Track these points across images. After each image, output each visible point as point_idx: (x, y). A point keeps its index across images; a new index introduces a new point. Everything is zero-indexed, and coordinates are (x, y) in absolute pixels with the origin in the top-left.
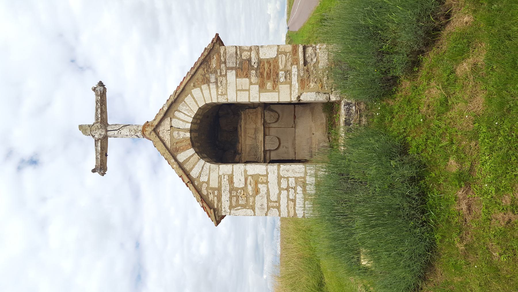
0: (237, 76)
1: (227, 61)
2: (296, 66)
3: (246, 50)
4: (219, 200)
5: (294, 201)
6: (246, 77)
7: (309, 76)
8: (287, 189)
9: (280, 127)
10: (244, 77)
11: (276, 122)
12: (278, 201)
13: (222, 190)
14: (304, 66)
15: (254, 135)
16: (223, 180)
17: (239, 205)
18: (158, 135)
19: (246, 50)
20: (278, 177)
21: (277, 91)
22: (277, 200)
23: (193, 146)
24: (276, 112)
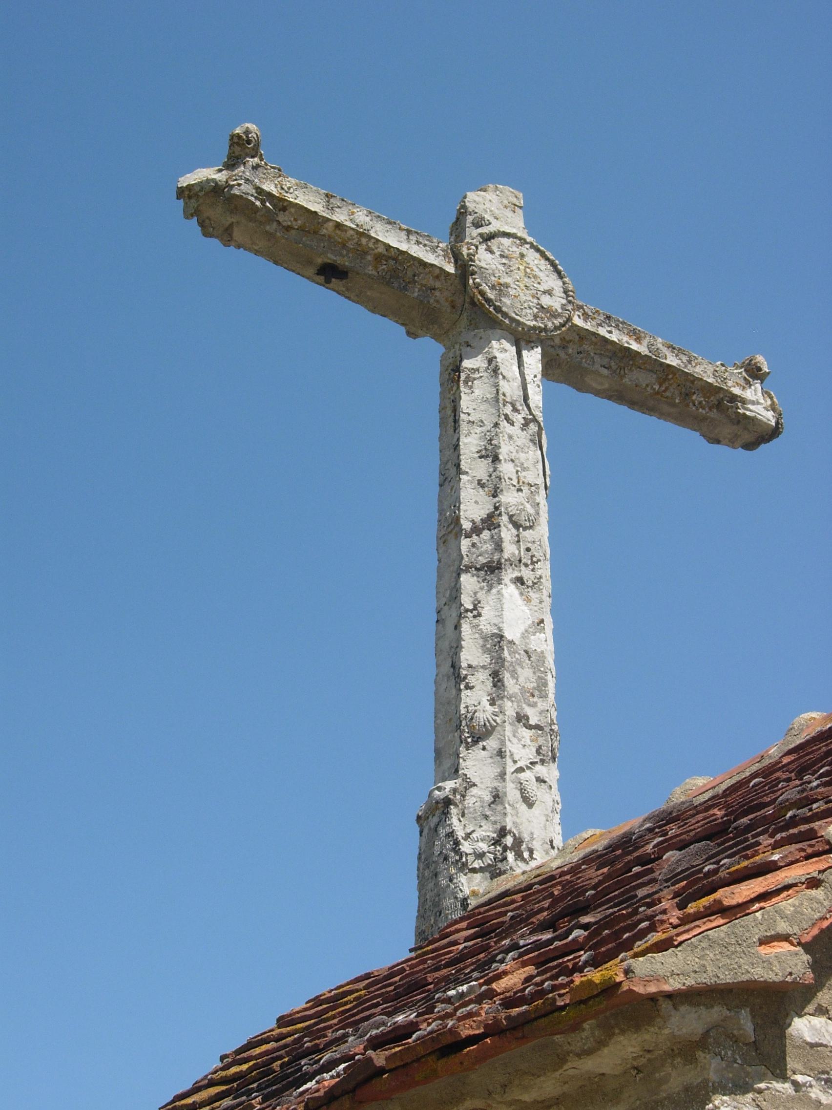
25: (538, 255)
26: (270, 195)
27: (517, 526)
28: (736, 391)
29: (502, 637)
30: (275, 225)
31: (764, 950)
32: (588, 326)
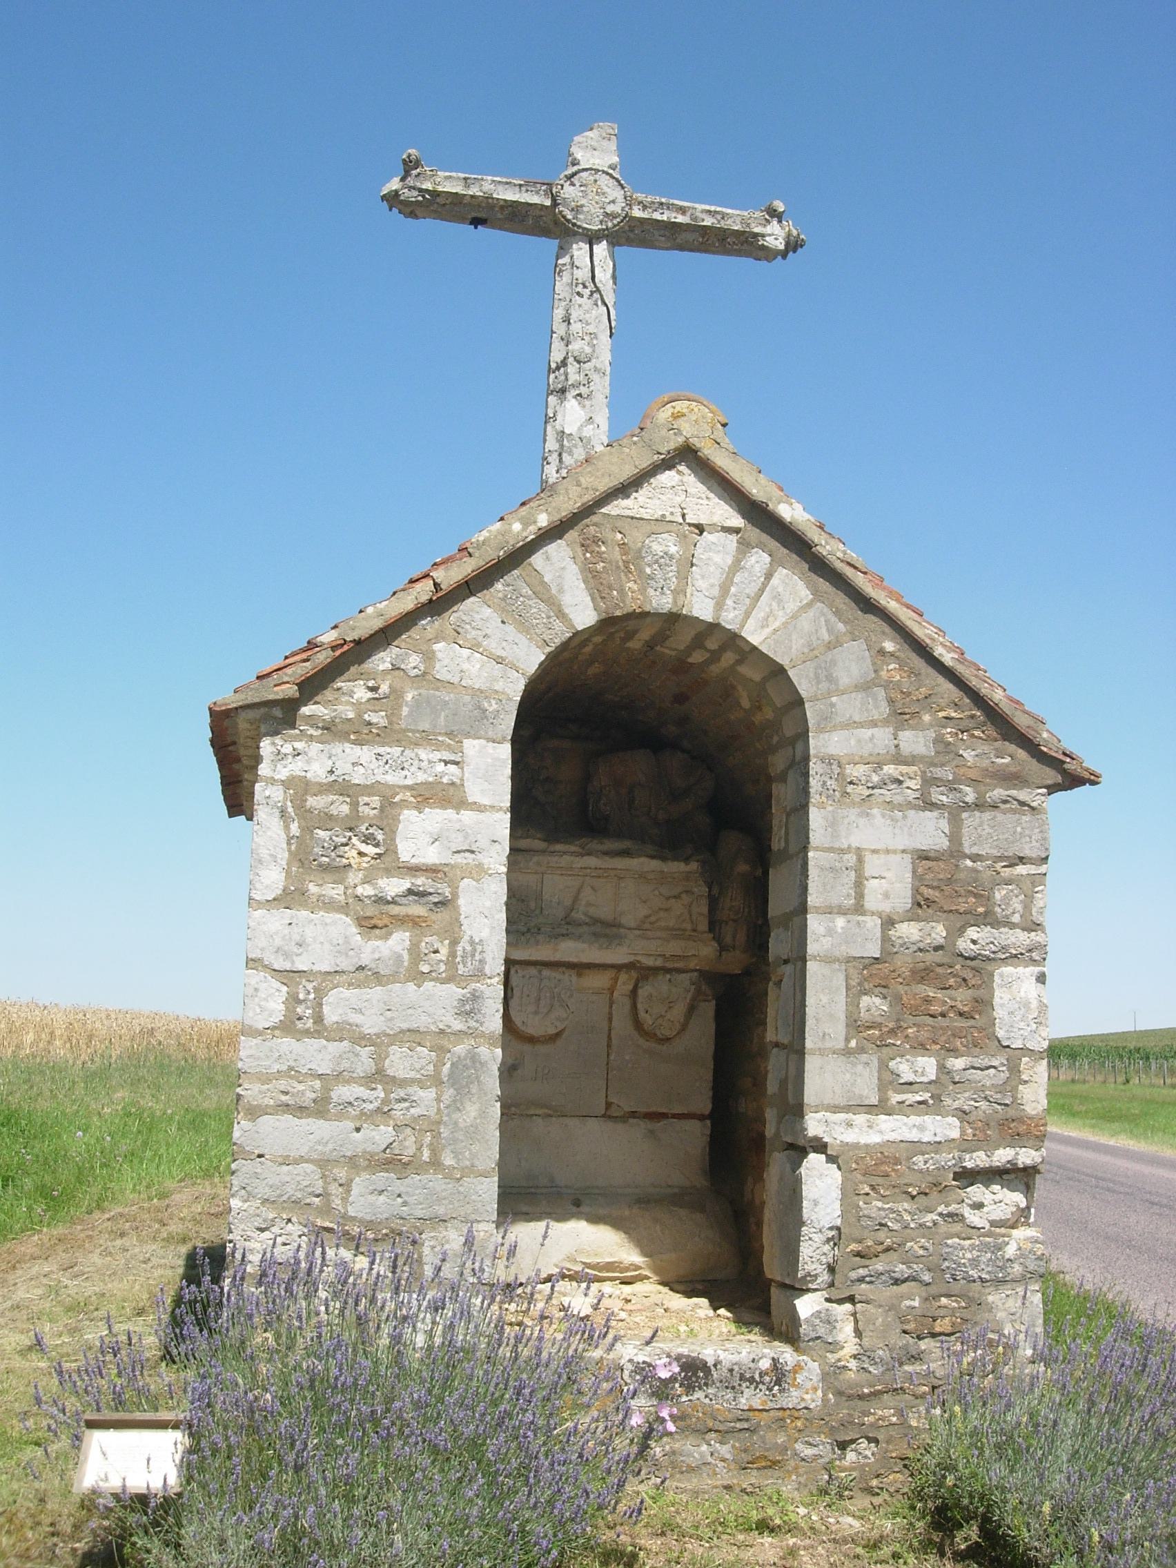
0: (923, 856)
1: (987, 815)
2: (955, 1134)
3: (1027, 906)
4: (331, 730)
5: (320, 1108)
6: (919, 897)
7: (913, 1197)
8: (378, 1076)
9: (609, 1046)
10: (916, 891)
11: (638, 1024)
12: (320, 1029)
13: (388, 749)
14: (955, 1173)
15: (585, 914)
16: (439, 757)
17: (308, 830)
18: (667, 464)
19: (1027, 906)
20: (442, 1032)
21: (853, 1043)
22: (325, 1022)
23: (607, 624)
24: (684, 1027)
25: (608, 177)
26: (427, 191)
27: (579, 362)
28: (756, 230)
29: (563, 432)
30: (436, 205)
31: (276, 689)
32: (645, 215)
